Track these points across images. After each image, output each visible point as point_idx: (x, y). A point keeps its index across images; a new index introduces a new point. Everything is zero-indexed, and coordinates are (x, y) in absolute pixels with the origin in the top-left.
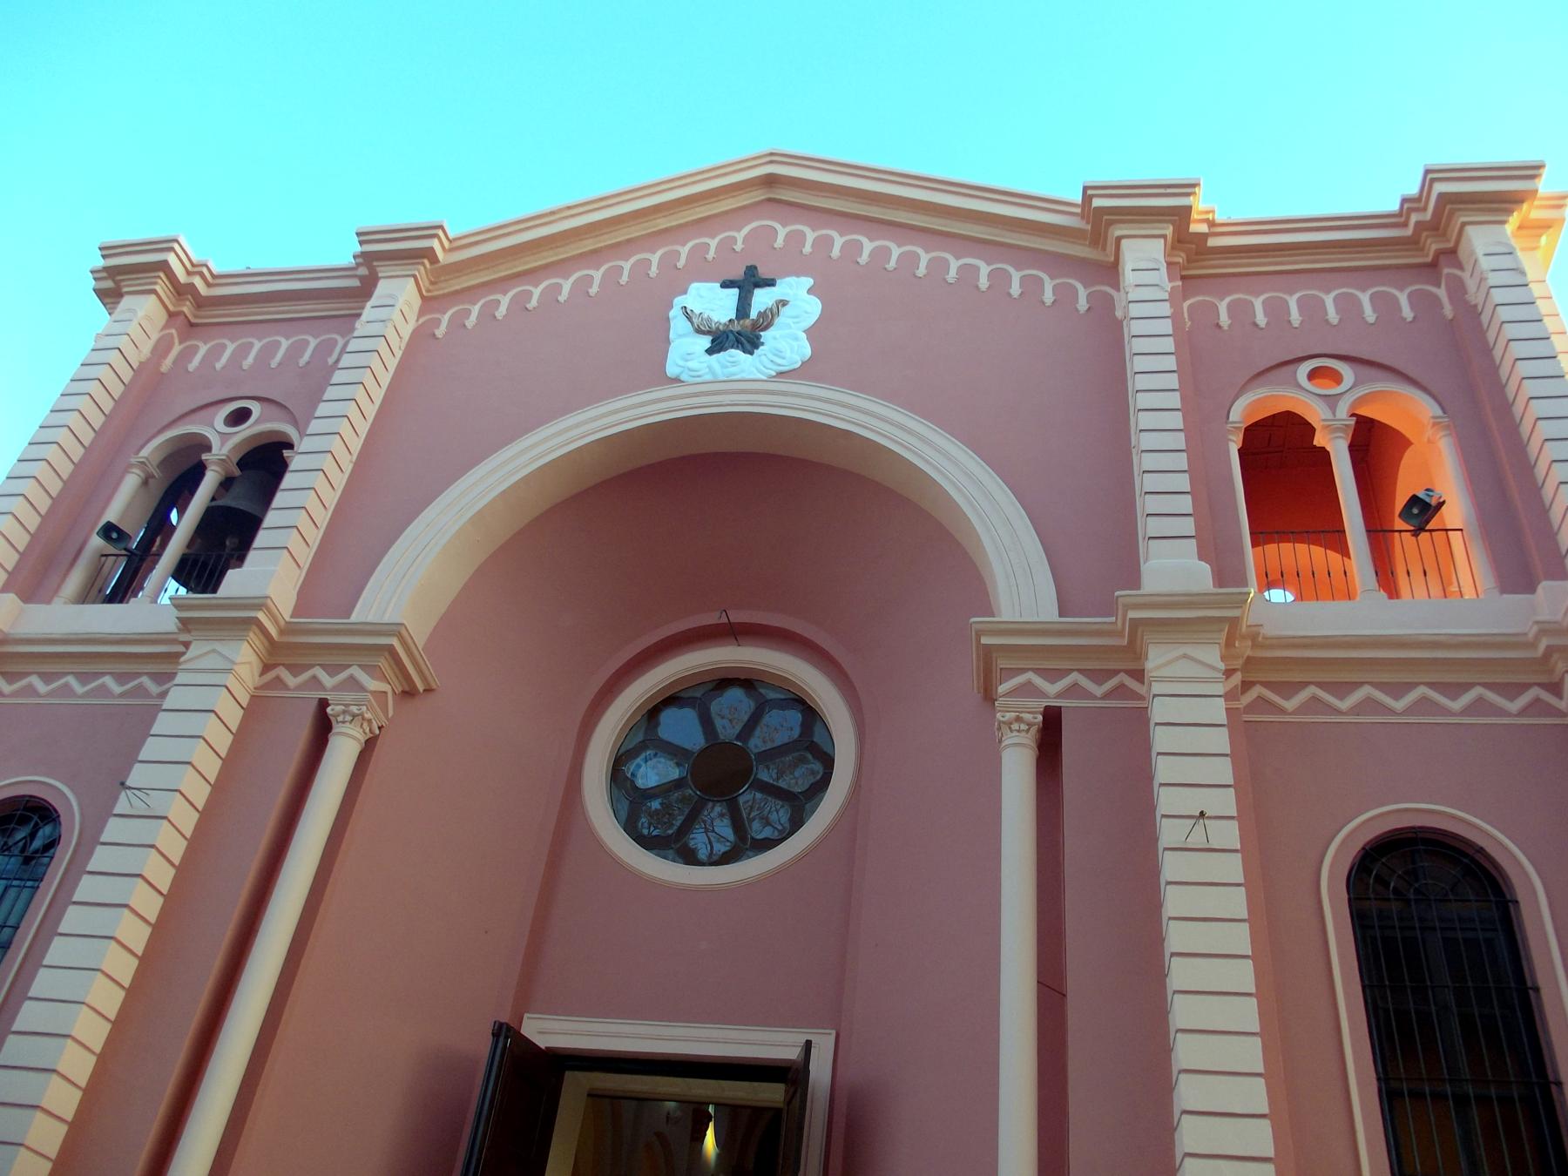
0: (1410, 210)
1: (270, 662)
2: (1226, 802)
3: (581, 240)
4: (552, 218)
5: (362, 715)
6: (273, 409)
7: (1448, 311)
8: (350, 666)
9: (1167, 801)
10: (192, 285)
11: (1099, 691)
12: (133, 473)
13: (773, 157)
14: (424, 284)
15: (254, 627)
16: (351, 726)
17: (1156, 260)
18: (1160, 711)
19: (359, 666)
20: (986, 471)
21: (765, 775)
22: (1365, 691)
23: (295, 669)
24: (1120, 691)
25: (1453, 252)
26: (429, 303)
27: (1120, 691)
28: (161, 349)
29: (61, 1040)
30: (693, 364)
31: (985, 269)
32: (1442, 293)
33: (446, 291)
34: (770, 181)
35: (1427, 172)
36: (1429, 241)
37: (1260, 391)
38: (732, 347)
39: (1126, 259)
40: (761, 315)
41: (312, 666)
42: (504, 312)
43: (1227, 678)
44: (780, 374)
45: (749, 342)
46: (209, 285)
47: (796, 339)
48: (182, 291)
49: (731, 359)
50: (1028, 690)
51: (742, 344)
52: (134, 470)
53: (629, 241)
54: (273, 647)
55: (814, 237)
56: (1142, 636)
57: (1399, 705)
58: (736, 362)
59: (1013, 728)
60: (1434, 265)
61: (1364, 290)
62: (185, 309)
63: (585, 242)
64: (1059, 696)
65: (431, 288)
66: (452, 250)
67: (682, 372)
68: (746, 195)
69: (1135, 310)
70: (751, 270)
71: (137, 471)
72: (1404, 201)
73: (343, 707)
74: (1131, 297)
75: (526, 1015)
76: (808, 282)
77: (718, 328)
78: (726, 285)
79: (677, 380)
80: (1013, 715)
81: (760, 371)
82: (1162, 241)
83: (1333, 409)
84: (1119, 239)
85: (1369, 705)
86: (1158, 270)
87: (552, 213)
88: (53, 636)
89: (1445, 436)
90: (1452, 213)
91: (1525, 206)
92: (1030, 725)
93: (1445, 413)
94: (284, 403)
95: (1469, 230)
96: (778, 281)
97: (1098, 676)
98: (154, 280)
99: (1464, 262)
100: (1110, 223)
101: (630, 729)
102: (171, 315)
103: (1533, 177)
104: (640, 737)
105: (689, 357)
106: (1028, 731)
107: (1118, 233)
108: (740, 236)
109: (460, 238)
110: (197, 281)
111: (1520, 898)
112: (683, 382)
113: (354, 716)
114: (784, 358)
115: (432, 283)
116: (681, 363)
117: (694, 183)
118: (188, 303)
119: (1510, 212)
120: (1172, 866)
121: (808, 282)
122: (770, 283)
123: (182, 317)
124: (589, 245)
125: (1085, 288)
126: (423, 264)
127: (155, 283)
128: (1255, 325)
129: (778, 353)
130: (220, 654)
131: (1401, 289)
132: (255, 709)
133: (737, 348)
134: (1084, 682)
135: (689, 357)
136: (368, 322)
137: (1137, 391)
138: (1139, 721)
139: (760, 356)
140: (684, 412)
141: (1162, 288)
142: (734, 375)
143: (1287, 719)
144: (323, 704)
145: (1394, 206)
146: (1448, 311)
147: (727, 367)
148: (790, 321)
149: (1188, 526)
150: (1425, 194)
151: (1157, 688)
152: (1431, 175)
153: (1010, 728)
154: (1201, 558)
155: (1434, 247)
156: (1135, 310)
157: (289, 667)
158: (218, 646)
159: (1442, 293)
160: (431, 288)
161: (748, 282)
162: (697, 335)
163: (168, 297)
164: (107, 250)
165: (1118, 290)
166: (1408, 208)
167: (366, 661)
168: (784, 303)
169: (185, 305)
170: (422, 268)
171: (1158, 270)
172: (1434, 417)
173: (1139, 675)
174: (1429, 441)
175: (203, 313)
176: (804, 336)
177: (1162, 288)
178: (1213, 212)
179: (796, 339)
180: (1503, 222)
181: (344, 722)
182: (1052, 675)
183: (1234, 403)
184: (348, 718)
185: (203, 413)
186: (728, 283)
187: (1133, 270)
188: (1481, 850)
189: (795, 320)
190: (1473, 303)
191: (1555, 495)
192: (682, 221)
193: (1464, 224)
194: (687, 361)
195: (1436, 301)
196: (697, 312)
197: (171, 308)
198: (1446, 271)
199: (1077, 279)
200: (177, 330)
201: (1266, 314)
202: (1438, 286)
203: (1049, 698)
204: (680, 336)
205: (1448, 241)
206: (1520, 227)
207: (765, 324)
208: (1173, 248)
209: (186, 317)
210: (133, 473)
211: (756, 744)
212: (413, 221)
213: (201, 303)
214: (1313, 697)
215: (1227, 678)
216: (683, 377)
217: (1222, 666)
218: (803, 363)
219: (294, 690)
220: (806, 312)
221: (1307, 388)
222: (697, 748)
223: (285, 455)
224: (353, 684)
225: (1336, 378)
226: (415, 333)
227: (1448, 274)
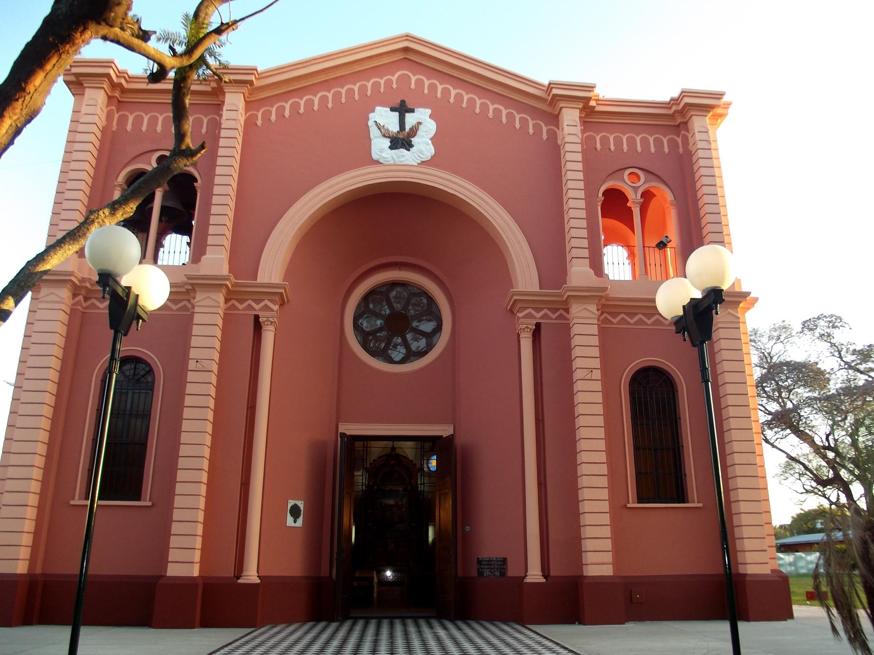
1: (228, 298)
2: (596, 363)
4: (306, 64)
5: (275, 322)
7: (681, 150)
8: (263, 300)
9: (577, 363)
10: (121, 84)
11: (554, 316)
13: (408, 37)
14: (247, 94)
15: (224, 287)
17: (575, 121)
19: (268, 300)
20: (515, 225)
21: (415, 324)
22: (640, 316)
23: (241, 301)
24: (561, 317)
25: (686, 123)
26: (249, 105)
27: (561, 317)
28: (109, 117)
29: (201, 458)
30: (384, 155)
31: (504, 112)
32: (679, 140)
34: (406, 50)
35: (682, 92)
36: (678, 117)
37: (610, 182)
38: (401, 148)
40: (411, 129)
41: (247, 300)
42: (289, 114)
45: (407, 144)
46: (127, 81)
47: (428, 144)
48: (114, 86)
49: (402, 154)
50: (529, 316)
51: (405, 145)
54: (229, 291)
55: (428, 83)
58: (403, 156)
60: (678, 126)
61: (651, 136)
62: (117, 95)
64: (541, 318)
65: (249, 96)
66: (259, 79)
67: (380, 159)
70: (403, 102)
71: (118, 188)
73: (266, 319)
75: (339, 424)
76: (428, 111)
77: (393, 136)
78: (392, 110)
79: (377, 162)
80: (525, 326)
81: (415, 162)
83: (636, 192)
84: (561, 108)
86: (576, 126)
87: (307, 62)
89: (674, 208)
90: (688, 110)
91: (715, 110)
92: (531, 329)
93: (675, 199)
95: (694, 118)
96: (416, 110)
97: (554, 310)
98: (103, 82)
99: (690, 131)
100: (558, 100)
101: (359, 306)
102: (109, 97)
103: (720, 99)
104: (363, 309)
105: (382, 151)
107: (561, 105)
108: (394, 78)
109: (263, 73)
110: (123, 81)
111: (679, 390)
113: (272, 322)
114: (424, 155)
115: (249, 94)
116: (379, 153)
118: (118, 92)
119: (710, 111)
120: (579, 386)
121: (428, 111)
122: (412, 111)
123: (116, 99)
125: (546, 127)
126: (247, 87)
127: (103, 84)
128: (610, 149)
129: (421, 152)
130: (211, 298)
131: (665, 137)
132: (228, 319)
133: (403, 148)
134: (549, 313)
135: (382, 151)
136: (227, 120)
139: (413, 153)
141: (578, 136)
142: (403, 162)
143: (615, 326)
144: (257, 318)
145: (667, 99)
146: (681, 150)
147: (399, 158)
148: (424, 134)
150: (680, 100)
152: (684, 93)
154: (591, 268)
155: (679, 121)
157: (237, 300)
158: (210, 295)
159: (679, 140)
160: (249, 96)
161: (402, 109)
162: (383, 138)
163: (108, 88)
167: (272, 298)
168: (419, 123)
170: (246, 89)
171: (576, 126)
172: (671, 201)
174: (668, 207)
175: (126, 96)
176: (430, 142)
177: (578, 136)
178: (598, 96)
179: (428, 144)
180: (706, 116)
182: (538, 310)
183: (600, 188)
184: (269, 323)
185: (144, 156)
186: (394, 109)
188: (669, 374)
189: (426, 133)
190: (691, 150)
191: (697, 171)
193: (692, 115)
194: (381, 152)
196: (382, 124)
197: (109, 94)
198: (683, 132)
199: (542, 121)
200: (115, 107)
201: (614, 145)
202: (679, 137)
204: (376, 137)
205: (685, 118)
206: (712, 115)
207: (414, 135)
209: (117, 99)
213: (124, 91)
216: (381, 161)
218: (431, 157)
220: (430, 130)
221: (626, 181)
223: (195, 185)
224: (266, 308)
225: (639, 178)
226: (246, 121)
227: (683, 134)
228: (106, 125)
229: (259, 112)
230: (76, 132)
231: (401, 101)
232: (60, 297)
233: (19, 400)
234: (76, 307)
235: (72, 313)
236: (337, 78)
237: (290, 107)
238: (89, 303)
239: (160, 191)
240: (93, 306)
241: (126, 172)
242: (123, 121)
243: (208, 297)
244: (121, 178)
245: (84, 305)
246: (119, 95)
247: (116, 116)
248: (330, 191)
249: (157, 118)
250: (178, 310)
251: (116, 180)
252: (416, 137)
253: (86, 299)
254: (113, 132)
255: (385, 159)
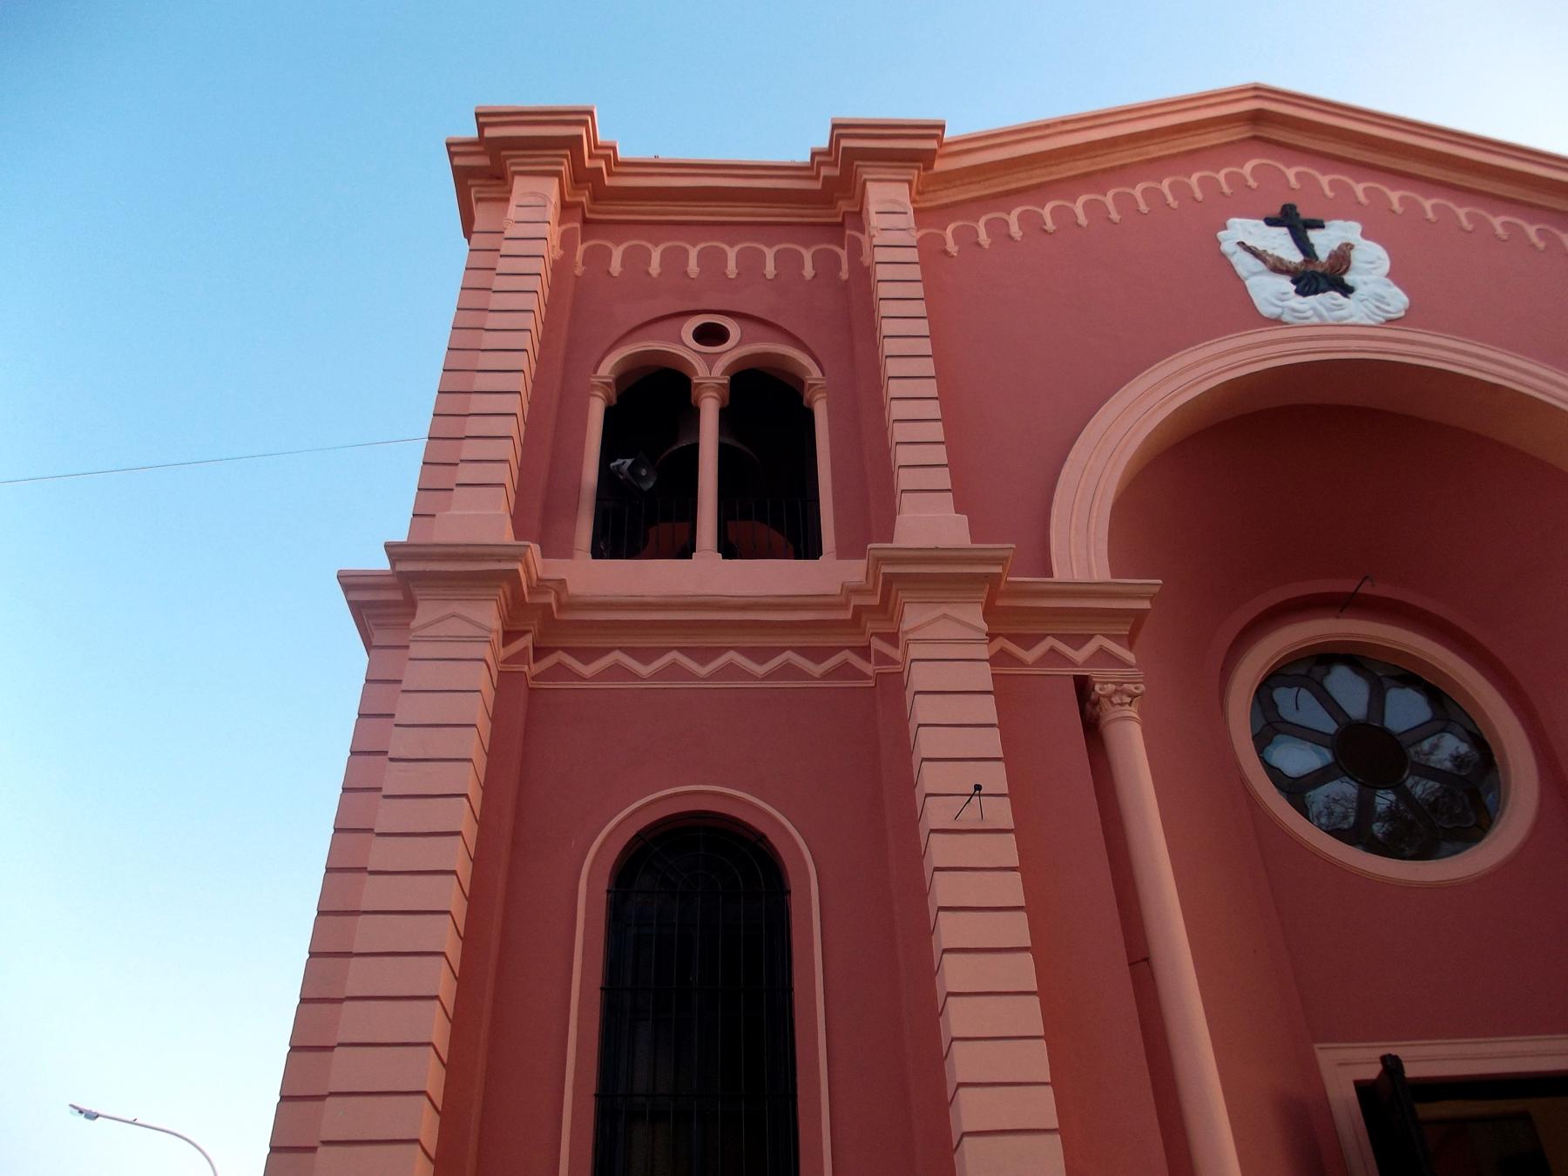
0: (607, 158)
2: (996, 777)
3: (1075, 160)
4: (1047, 132)
6: (752, 328)
8: (1091, 637)
9: (931, 778)
12: (818, 399)
13: (1259, 91)
16: (1129, 708)
18: (921, 677)
19: (1103, 635)
28: (566, 241)
33: (934, 204)
34: (1257, 117)
39: (871, 200)
43: (991, 641)
44: (1390, 321)
48: (583, 177)
52: (819, 396)
53: (1123, 167)
56: (897, 594)
57: (588, 670)
58: (1324, 304)
59: (1115, 702)
63: (1079, 163)
65: (917, 198)
67: (1283, 313)
68: (1233, 130)
69: (881, 255)
72: (814, 154)
73: (1114, 687)
74: (875, 241)
78: (1271, 222)
81: (1373, 319)
82: (907, 186)
85: (674, 671)
86: (905, 213)
87: (1047, 126)
88: (645, 599)
94: (773, 320)
106: (1130, 704)
112: (1286, 323)
113: (1133, 696)
114: (1389, 305)
116: (1280, 304)
117: (1185, 110)
124: (1082, 166)
127: (561, 164)
132: (1005, 691)
137: (884, 337)
138: (893, 687)
139: (1362, 301)
140: (1318, 355)
142: (1345, 318)
144: (1083, 686)
145: (804, 157)
147: (1332, 310)
149: (943, 478)
151: (915, 651)
153: (1112, 702)
156: (881, 255)
160: (917, 198)
162: (1273, 274)
164: (485, 118)
165: (863, 232)
166: (818, 163)
169: (584, 195)
171: (905, 213)
173: (892, 638)
181: (1122, 704)
187: (877, 213)
192: (1175, 151)
194: (1283, 301)
195: (837, 258)
203: (1077, 666)
208: (919, 193)
210: (818, 399)
211: (1329, 726)
212: (496, 104)
213: (602, 195)
214: (558, 663)
215: (991, 641)
216: (1287, 317)
217: (985, 626)
219: (1032, 666)
222: (1332, 732)
224: (1104, 657)
228: (562, 258)
229: (945, 229)
230: (363, 870)
231: (1284, 207)
232: (481, 626)
233: (494, 269)
234: (516, 667)
235: (505, 681)
236: (1112, 169)
237: (1018, 220)
238: (548, 662)
239: (714, 397)
240: (561, 671)
241: (618, 359)
242: (598, 258)
243: (945, 616)
244: (607, 369)
245: (536, 668)
246: (587, 201)
247: (581, 249)
248: (1184, 379)
249: (686, 252)
250: (826, 676)
251: (595, 372)
252: (1349, 273)
253: (540, 652)
254: (577, 277)
255: (1296, 314)
